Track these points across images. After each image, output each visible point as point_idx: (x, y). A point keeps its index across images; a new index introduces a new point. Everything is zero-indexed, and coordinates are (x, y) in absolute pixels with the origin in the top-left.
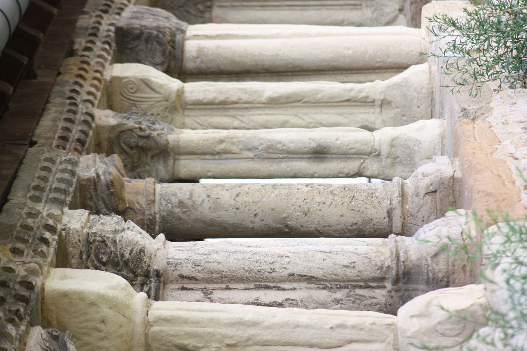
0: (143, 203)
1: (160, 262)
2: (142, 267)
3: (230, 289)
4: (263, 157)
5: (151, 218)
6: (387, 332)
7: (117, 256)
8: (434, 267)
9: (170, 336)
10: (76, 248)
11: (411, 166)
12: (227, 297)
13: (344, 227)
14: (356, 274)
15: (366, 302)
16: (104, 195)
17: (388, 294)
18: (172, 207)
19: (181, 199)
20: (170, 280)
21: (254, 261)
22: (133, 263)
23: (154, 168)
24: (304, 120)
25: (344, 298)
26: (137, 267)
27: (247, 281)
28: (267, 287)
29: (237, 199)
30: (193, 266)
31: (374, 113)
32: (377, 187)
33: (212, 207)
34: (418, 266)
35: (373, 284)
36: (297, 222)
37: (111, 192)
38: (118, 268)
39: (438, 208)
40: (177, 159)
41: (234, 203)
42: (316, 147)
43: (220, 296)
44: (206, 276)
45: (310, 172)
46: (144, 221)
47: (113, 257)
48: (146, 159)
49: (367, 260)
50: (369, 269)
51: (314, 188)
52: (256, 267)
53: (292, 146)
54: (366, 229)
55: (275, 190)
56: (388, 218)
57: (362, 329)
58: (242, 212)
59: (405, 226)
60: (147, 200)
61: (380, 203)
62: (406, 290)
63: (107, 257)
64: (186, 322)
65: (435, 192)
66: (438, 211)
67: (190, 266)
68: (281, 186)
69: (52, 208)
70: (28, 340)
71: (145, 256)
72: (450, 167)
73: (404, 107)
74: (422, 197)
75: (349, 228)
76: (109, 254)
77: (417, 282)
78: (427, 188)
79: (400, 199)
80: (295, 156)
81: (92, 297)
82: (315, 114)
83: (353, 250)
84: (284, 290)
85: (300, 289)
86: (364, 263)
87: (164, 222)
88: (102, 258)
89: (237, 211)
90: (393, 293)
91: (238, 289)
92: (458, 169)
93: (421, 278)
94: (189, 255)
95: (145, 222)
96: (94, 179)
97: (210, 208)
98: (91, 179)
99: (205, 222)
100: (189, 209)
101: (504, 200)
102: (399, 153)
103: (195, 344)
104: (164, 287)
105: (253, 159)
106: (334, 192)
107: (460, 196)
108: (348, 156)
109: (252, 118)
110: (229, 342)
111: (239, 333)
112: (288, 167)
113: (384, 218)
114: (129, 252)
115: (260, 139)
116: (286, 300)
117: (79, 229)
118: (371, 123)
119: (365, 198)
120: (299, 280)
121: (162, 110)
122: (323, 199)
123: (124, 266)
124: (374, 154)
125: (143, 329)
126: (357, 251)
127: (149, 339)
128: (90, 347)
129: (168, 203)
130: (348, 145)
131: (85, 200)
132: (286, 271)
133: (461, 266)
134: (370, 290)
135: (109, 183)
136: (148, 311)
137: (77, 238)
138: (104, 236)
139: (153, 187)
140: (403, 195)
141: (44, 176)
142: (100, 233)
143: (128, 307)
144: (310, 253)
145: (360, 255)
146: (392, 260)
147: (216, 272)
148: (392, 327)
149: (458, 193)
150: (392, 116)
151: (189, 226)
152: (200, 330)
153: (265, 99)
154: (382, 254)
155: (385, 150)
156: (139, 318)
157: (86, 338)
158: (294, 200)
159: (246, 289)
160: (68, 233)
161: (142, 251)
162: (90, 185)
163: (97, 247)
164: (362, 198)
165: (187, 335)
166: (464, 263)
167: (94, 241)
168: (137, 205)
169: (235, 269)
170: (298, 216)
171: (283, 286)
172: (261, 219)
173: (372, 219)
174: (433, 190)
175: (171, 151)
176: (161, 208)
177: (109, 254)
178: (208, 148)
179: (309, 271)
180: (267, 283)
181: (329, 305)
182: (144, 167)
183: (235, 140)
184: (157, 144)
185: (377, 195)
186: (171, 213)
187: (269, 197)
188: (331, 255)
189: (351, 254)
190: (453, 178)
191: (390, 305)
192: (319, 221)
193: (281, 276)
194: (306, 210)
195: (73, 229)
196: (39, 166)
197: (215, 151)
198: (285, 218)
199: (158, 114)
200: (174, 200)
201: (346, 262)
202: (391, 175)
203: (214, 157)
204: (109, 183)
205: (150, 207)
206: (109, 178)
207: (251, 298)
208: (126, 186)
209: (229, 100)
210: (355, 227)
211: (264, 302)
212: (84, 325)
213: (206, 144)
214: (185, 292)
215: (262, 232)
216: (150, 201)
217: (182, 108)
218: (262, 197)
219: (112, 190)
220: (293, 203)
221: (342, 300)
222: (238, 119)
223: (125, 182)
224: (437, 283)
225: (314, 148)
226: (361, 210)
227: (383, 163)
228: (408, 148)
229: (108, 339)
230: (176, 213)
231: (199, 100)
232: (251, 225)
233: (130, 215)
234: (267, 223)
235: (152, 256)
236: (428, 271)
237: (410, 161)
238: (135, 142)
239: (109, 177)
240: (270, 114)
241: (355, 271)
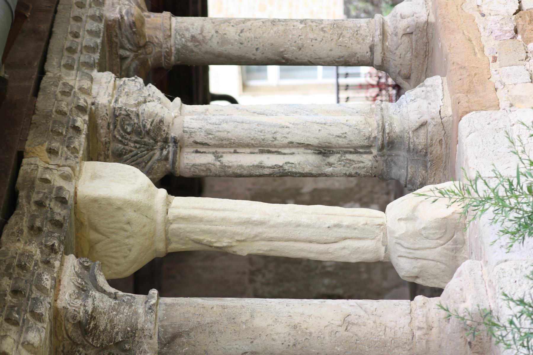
0: (161, 38)
1: (176, 129)
2: (161, 135)
3: (238, 153)
5: (168, 50)
6: (377, 231)
7: (140, 127)
8: (415, 139)
10: (105, 120)
12: (235, 160)
15: (355, 165)
16: (127, 33)
17: (374, 159)
18: (185, 41)
19: (193, 34)
20: (186, 145)
21: (259, 131)
22: (153, 132)
25: (336, 162)
26: (157, 135)
28: (269, 152)
29: (241, 34)
32: (362, 25)
34: (401, 137)
35: (361, 150)
37: (133, 31)
38: (141, 137)
39: (413, 48)
41: (239, 39)
43: (229, 159)
44: (217, 143)
47: (136, 127)
49: (357, 132)
50: (358, 138)
51: (307, 25)
52: (260, 136)
55: (274, 26)
57: (355, 229)
58: (245, 47)
59: (385, 60)
60: (164, 35)
61: (363, 40)
63: (131, 127)
64: (201, 220)
65: (412, 33)
66: (413, 50)
67: (203, 134)
68: (279, 23)
69: (83, 79)
70: (62, 276)
72: (425, 9)
74: (400, 37)
75: (337, 60)
76: (133, 126)
77: (399, 149)
78: (405, 30)
79: (381, 37)
81: (119, 203)
83: (345, 122)
84: (285, 154)
85: (298, 153)
86: (354, 134)
88: (127, 128)
89: (241, 46)
90: (378, 158)
91: (244, 153)
92: (431, 10)
93: (403, 147)
94: (202, 125)
95: (163, 53)
96: (119, 20)
97: (218, 43)
98: (116, 20)
99: (214, 54)
100: (200, 43)
101: (475, 74)
103: (209, 239)
104: (180, 150)
106: (325, 29)
107: (432, 37)
110: (239, 238)
111: (248, 231)
113: (367, 52)
114: (150, 123)
116: (286, 163)
117: (107, 105)
119: (351, 35)
122: (315, 36)
123: (146, 134)
125: (164, 227)
126: (348, 123)
128: (118, 244)
129: (182, 38)
131: (111, 37)
132: (287, 140)
133: (438, 140)
134: (358, 155)
135: (132, 24)
136: (167, 209)
137: (105, 112)
138: (128, 110)
139: (169, 23)
140: (384, 33)
141: (76, 32)
142: (124, 108)
143: (150, 208)
144: (307, 124)
145: (350, 126)
146: (378, 132)
147: (225, 140)
148: (382, 227)
149: (430, 35)
151: (200, 57)
152: (214, 228)
154: (370, 126)
156: (160, 218)
157: (114, 237)
158: (290, 36)
159: (251, 153)
160: (97, 108)
161: (161, 121)
162: (116, 25)
163: (123, 120)
164: (348, 35)
165: (202, 232)
166: (441, 138)
167: (120, 114)
168: (155, 39)
171: (283, 151)
172: (262, 52)
174: (410, 32)
176: (176, 42)
177: (133, 126)
179: (306, 140)
180: (269, 149)
185: (361, 32)
186: (185, 47)
187: (269, 33)
188: (326, 126)
189: (343, 126)
190: (427, 23)
191: (375, 168)
192: (311, 55)
194: (300, 45)
195: (102, 104)
196: (71, 16)
198: (282, 52)
200: (188, 35)
201: (338, 133)
204: (132, 24)
205: (167, 41)
206: (132, 19)
207: (255, 161)
208: (146, 22)
210: (342, 59)
211: (267, 165)
212: (111, 226)
214: (199, 154)
218: (263, 33)
219: (134, 30)
220: (289, 39)
221: (334, 164)
223: (145, 17)
224: (417, 153)
226: (348, 45)
229: (133, 237)
230: (189, 46)
233: (149, 47)
234: (267, 55)
235: (170, 124)
236: (409, 143)
239: (131, 18)
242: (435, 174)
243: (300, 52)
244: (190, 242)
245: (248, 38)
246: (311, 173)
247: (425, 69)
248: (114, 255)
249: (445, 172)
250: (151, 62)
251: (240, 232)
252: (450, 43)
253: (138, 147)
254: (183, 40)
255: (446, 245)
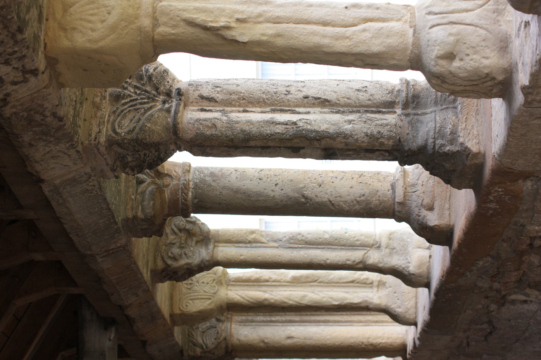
2: (164, 85)
4: (286, 246)
6: (404, 11)
9: (179, 11)
11: (405, 255)
13: (353, 198)
14: (368, 98)
18: (204, 176)
22: (156, 78)
23: (197, 251)
24: (319, 295)
27: (263, 105)
30: (213, 87)
31: (372, 292)
33: (238, 177)
36: (312, 192)
40: (216, 246)
42: (328, 238)
44: (225, 97)
45: (323, 258)
46: (179, 185)
48: (192, 243)
50: (380, 92)
53: (310, 237)
54: (373, 201)
56: (391, 191)
57: (378, 9)
59: (407, 195)
60: (183, 169)
62: (415, 114)
67: (210, 87)
71: (168, 77)
73: (396, 286)
75: (358, 199)
77: (425, 106)
80: (312, 246)
82: (328, 291)
85: (314, 113)
87: (196, 189)
89: (260, 181)
90: (403, 117)
91: (254, 112)
97: (237, 178)
99: (232, 189)
102: (395, 245)
103: (204, 18)
105: (277, 247)
108: (354, 248)
109: (281, 293)
110: (240, 16)
111: (251, 9)
112: (306, 254)
113: (389, 191)
115: (284, 233)
118: (370, 298)
120: (314, 104)
121: (211, 280)
122: (335, 175)
123: (148, 83)
124: (375, 246)
127: (157, 13)
128: (96, 5)
130: (354, 237)
147: (234, 93)
148: (409, 8)
150: (386, 293)
151: (218, 193)
153: (290, 278)
155: (384, 243)
158: (310, 175)
168: (174, 173)
169: (253, 90)
170: (313, 186)
171: (297, 109)
172: (281, 188)
173: (378, 191)
175: (212, 238)
178: (241, 236)
179: (323, 94)
181: (341, 125)
182: (189, 248)
183: (264, 233)
184: (201, 230)
186: (203, 181)
191: (400, 127)
192: (331, 192)
193: (296, 99)
197: (247, 239)
198: (302, 188)
199: (208, 283)
202: (389, 263)
203: (246, 245)
209: (262, 278)
210: (363, 198)
213: (240, 233)
215: (281, 201)
216: (185, 170)
217: (226, 283)
221: (354, 121)
222: (268, 293)
225: (327, 239)
226: (369, 183)
227: (383, 253)
228: (403, 240)
230: (207, 181)
231: (240, 277)
232: (272, 194)
237: (404, 250)
238: (183, 225)
240: (293, 291)
241: (367, 95)
242: (466, 118)
243: (320, 188)
244: (182, 24)
245: (268, 175)
246: (328, 132)
247: (448, 197)
248: (91, 18)
249: (478, 117)
250: (168, 195)
251: (241, 10)
252: (470, 61)
253: (138, 93)
254: (202, 175)
255: (486, 6)
